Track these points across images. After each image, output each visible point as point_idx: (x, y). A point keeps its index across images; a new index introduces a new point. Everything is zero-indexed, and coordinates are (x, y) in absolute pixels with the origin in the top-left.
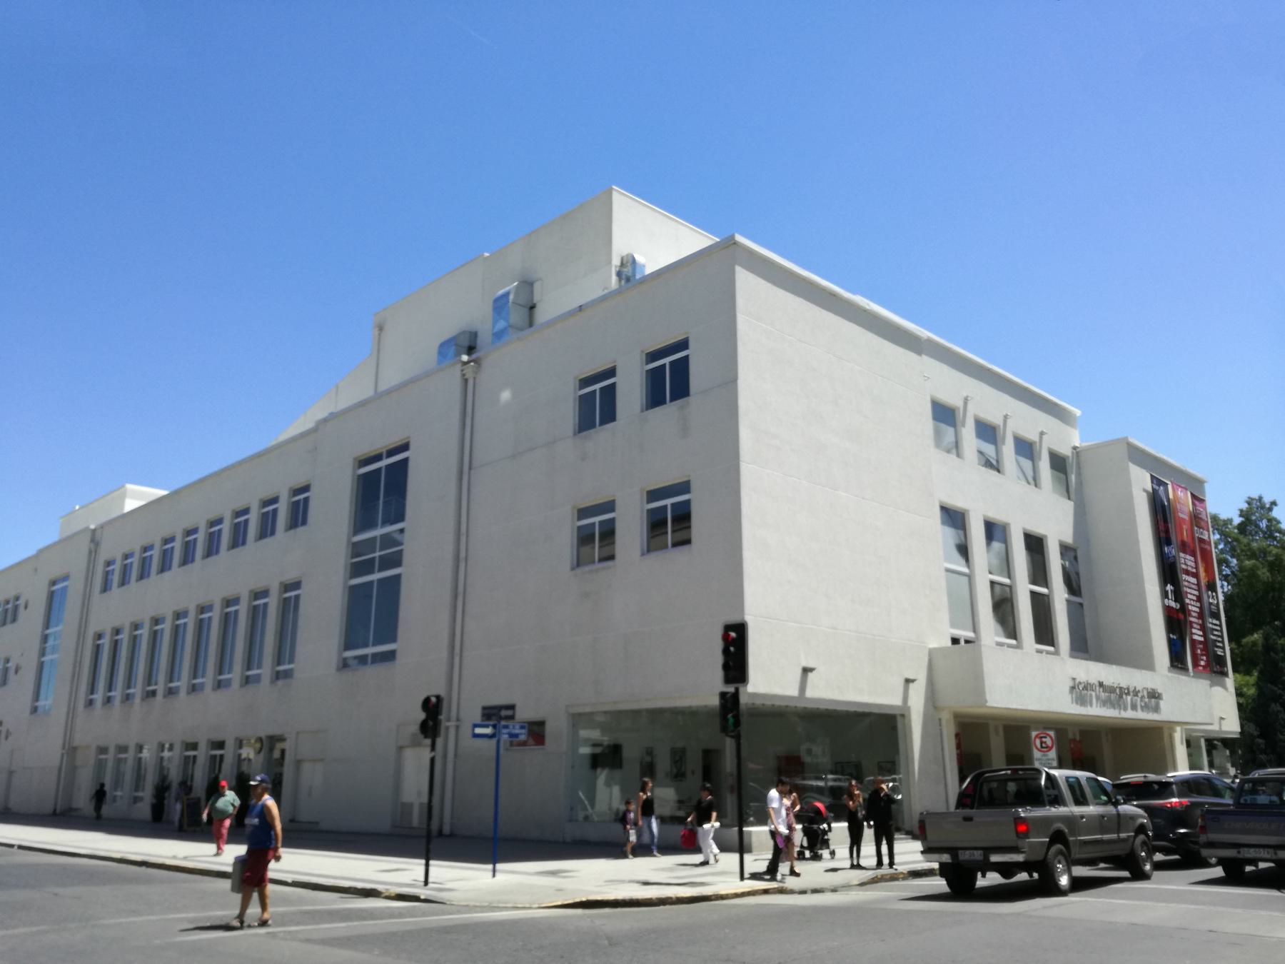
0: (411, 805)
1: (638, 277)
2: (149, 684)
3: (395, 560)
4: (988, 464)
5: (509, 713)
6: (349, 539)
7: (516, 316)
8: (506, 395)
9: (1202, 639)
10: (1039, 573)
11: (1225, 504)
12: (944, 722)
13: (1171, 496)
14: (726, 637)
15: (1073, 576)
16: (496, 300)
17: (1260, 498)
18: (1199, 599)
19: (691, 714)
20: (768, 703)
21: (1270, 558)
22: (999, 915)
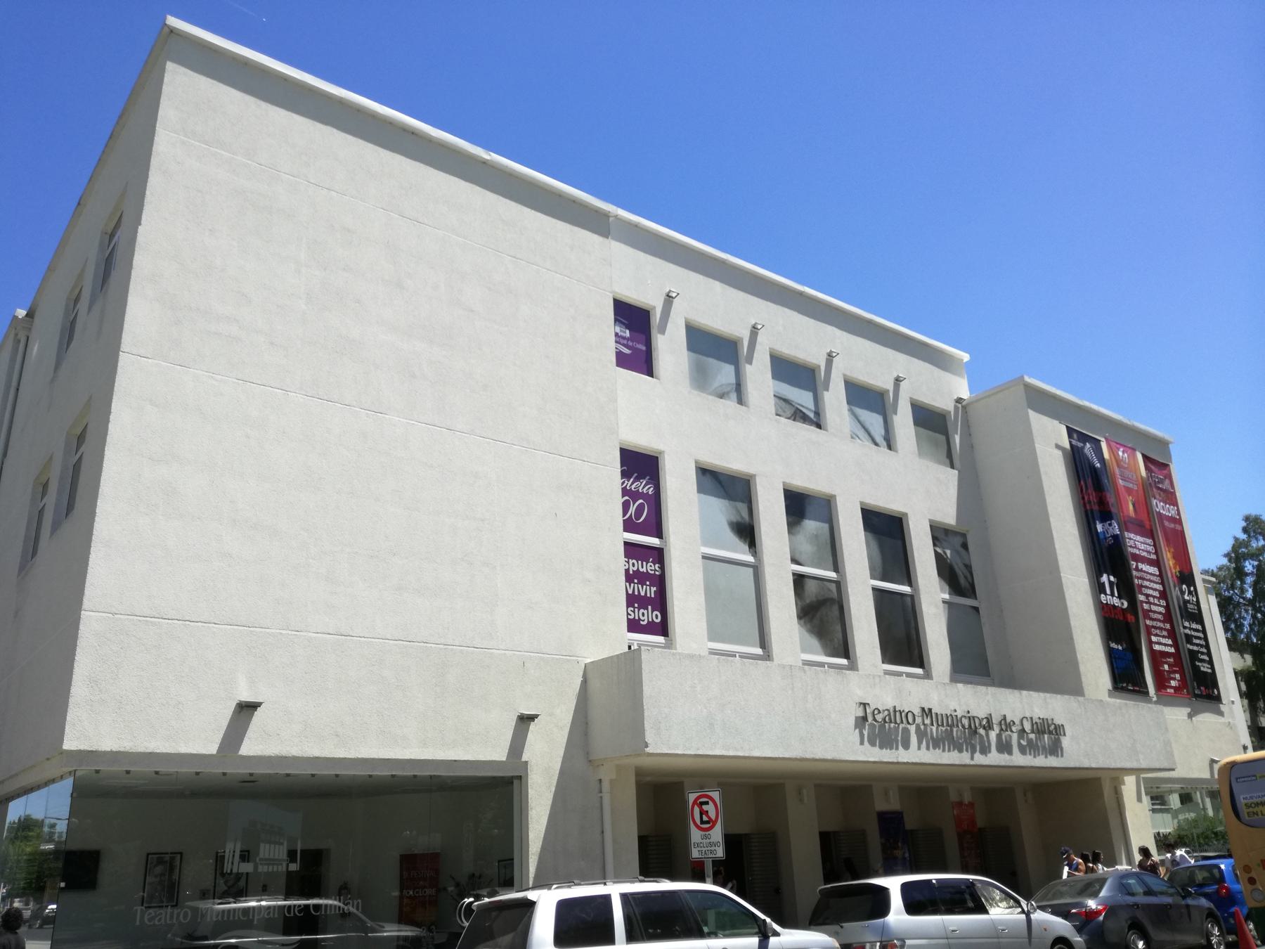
4: (799, 415)
9: (1172, 650)
12: (606, 786)
13: (1106, 455)
18: (1164, 595)
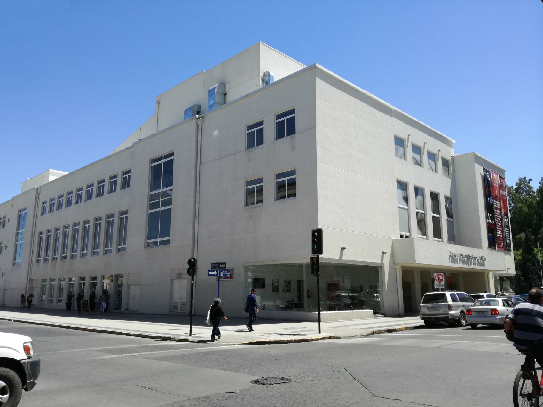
0: (177, 303)
1: (271, 82)
2: (64, 253)
3: (169, 202)
4: (417, 163)
5: (224, 266)
6: (148, 193)
7: (218, 98)
8: (216, 133)
10: (436, 209)
11: (511, 182)
14: (313, 235)
15: (450, 210)
16: (209, 91)
17: (525, 178)
19: (301, 266)
20: (327, 262)
21: (528, 203)
22: (430, 348)
